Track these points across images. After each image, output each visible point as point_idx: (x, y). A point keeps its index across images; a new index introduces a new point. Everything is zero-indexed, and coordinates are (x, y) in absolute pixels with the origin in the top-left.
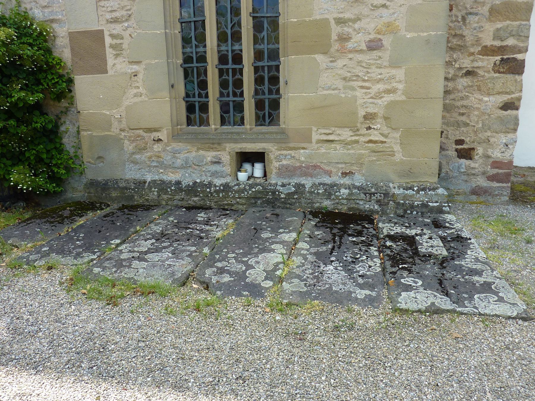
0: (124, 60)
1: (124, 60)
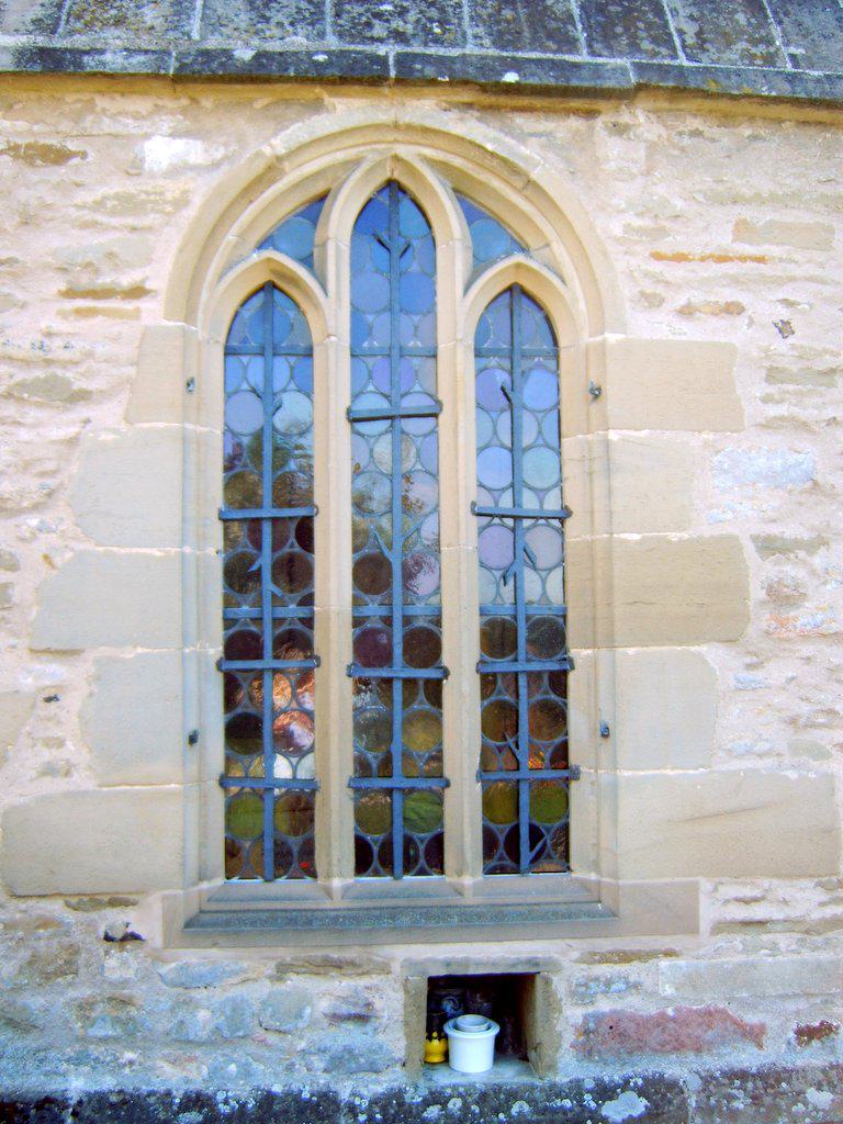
0: (13, 641)
1: (13, 641)
